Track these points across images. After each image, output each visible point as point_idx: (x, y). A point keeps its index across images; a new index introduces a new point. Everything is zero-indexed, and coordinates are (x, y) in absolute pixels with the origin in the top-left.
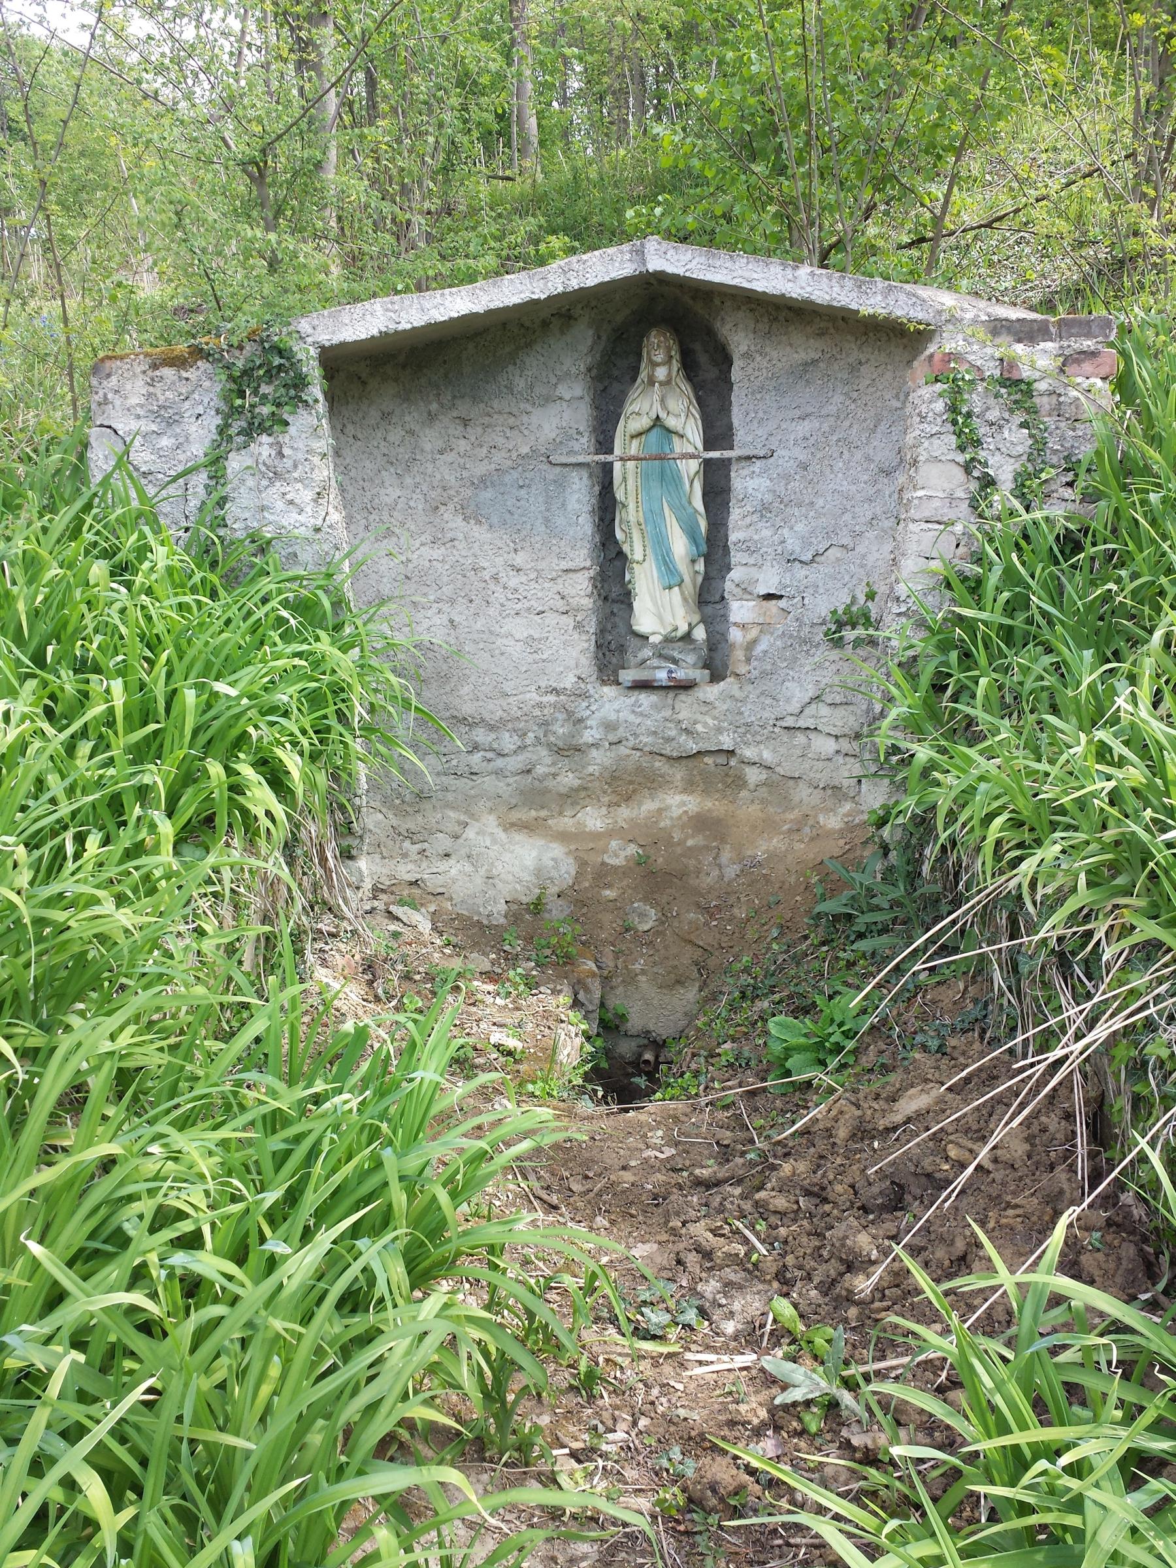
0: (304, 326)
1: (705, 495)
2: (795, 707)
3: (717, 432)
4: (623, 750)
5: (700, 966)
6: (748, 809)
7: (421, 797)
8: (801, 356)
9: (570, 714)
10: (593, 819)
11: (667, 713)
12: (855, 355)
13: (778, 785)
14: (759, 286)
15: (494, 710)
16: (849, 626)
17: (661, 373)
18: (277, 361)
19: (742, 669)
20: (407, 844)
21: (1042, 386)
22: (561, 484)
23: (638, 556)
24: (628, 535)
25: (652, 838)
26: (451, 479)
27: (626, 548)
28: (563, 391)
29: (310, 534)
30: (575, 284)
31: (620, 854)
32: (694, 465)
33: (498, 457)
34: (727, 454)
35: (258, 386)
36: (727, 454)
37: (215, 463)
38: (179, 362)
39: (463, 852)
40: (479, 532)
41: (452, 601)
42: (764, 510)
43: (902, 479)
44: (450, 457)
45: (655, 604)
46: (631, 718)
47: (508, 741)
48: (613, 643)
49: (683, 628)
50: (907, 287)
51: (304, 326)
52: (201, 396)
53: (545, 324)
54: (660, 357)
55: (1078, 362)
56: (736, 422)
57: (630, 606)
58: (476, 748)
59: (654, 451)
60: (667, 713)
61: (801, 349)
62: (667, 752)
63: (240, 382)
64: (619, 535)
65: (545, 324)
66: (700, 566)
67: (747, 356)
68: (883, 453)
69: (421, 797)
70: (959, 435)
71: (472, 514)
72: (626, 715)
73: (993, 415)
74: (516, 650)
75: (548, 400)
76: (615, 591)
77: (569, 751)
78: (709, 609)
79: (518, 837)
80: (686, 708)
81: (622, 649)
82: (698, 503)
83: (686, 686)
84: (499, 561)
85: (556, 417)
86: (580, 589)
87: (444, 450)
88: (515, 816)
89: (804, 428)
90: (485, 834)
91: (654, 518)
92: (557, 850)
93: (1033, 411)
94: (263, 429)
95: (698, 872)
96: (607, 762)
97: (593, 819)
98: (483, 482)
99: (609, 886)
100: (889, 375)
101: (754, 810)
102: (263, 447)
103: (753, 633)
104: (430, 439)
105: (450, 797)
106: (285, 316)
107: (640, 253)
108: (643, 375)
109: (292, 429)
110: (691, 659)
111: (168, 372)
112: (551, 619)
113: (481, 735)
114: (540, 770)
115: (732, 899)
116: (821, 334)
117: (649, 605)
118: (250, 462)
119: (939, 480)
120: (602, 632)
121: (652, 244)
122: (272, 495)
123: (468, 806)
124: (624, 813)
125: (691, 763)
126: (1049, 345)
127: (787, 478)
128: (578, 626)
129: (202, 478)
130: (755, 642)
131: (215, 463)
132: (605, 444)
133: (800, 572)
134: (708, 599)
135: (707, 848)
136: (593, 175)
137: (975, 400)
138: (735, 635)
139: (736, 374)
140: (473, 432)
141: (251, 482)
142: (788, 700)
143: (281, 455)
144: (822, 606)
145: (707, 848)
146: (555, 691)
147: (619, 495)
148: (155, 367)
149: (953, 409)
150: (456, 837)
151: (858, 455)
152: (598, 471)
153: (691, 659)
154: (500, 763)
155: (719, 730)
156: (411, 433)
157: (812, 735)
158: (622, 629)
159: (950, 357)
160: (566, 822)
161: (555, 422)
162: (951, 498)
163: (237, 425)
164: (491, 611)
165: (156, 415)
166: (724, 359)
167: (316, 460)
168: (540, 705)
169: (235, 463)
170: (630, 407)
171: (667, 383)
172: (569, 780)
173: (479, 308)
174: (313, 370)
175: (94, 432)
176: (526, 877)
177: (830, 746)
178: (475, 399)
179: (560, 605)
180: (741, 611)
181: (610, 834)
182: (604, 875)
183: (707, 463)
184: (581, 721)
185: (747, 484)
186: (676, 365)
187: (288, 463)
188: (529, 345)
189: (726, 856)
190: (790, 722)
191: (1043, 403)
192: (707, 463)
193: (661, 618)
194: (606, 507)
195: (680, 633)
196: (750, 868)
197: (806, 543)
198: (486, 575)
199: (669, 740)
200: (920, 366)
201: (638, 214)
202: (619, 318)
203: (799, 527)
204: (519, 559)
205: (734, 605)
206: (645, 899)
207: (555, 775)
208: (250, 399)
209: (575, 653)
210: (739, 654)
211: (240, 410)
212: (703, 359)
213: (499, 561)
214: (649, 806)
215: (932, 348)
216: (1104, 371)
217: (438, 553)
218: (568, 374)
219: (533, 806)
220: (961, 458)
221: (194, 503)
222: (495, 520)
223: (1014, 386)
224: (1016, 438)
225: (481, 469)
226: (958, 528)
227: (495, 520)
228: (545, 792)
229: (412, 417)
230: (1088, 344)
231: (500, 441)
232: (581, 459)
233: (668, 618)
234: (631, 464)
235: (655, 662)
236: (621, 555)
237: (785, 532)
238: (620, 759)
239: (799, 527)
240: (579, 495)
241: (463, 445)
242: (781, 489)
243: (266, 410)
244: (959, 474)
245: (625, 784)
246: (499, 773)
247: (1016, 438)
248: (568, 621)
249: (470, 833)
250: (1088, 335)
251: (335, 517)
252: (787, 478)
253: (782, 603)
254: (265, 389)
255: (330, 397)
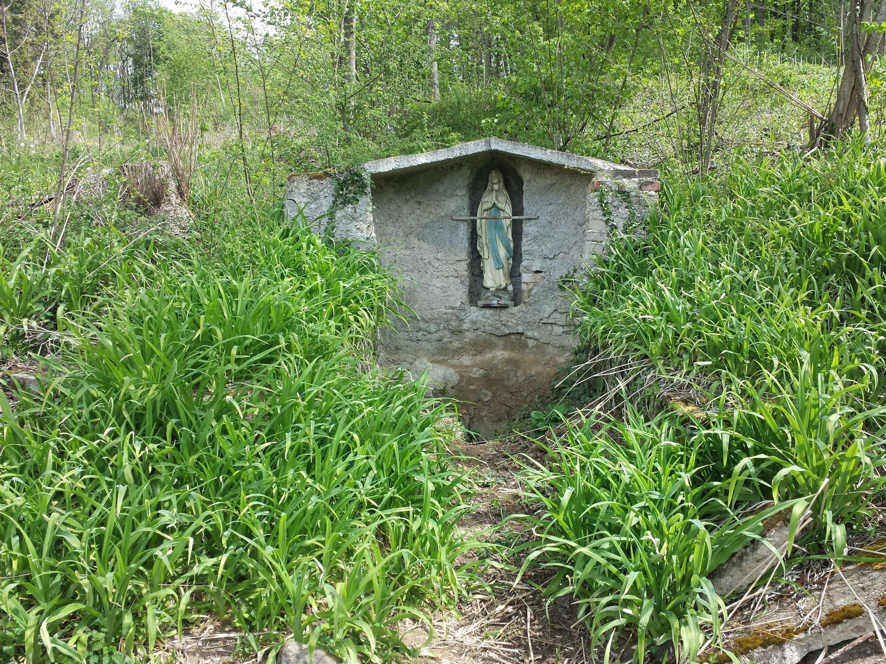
0: (366, 166)
1: (513, 234)
2: (547, 315)
3: (517, 209)
4: (479, 333)
5: (508, 414)
6: (528, 356)
7: (397, 348)
8: (549, 182)
9: (458, 317)
10: (466, 360)
11: (497, 317)
12: (569, 182)
13: (541, 346)
14: (533, 156)
15: (428, 315)
16: (565, 283)
17: (496, 187)
18: (356, 178)
19: (527, 300)
20: (392, 365)
21: (633, 194)
22: (456, 227)
23: (486, 256)
24: (482, 248)
25: (489, 368)
26: (414, 224)
27: (481, 253)
28: (458, 192)
29: (365, 240)
30: (464, 153)
31: (477, 373)
32: (508, 222)
33: (432, 216)
34: (521, 217)
35: (348, 187)
36: (521, 217)
37: (331, 214)
38: (319, 178)
39: (414, 370)
40: (424, 245)
41: (412, 271)
42: (535, 239)
43: (584, 227)
44: (413, 216)
45: (492, 274)
46: (483, 319)
47: (433, 328)
48: (475, 289)
49: (504, 285)
50: (585, 158)
51: (366, 166)
52: (326, 192)
53: (452, 168)
54: (495, 182)
55: (646, 185)
56: (524, 206)
57: (483, 277)
58: (420, 330)
59: (493, 216)
60: (497, 317)
61: (550, 180)
62: (497, 333)
63: (342, 185)
64: (478, 248)
65: (452, 168)
66: (511, 261)
67: (529, 181)
68: (579, 219)
69: (397, 348)
70: (603, 210)
71: (421, 238)
72: (480, 318)
73: (615, 204)
74: (437, 291)
75: (452, 196)
76: (477, 271)
77: (457, 332)
78: (514, 279)
79: (436, 365)
80: (504, 315)
81: (479, 294)
82: (510, 237)
83: (505, 307)
84: (431, 256)
85: (456, 202)
86: (463, 268)
87: (412, 214)
88: (434, 358)
89: (550, 208)
90: (423, 363)
91: (492, 241)
92: (452, 371)
93: (630, 202)
94: (349, 202)
95: (508, 379)
96: (472, 337)
97: (466, 360)
98: (426, 226)
99: (472, 384)
100: (581, 189)
101: (531, 357)
102: (349, 209)
103: (531, 286)
104: (406, 209)
105: (409, 349)
106: (357, 162)
107: (489, 143)
108: (489, 187)
109: (360, 203)
110: (506, 297)
111: (315, 181)
112: (451, 279)
113: (422, 325)
114: (445, 340)
115: (521, 389)
116: (556, 174)
117: (490, 276)
118: (344, 214)
119: (596, 226)
120: (471, 286)
121: (493, 140)
122: (352, 226)
123: (416, 355)
124: (479, 358)
125: (506, 338)
126: (636, 179)
127: (544, 227)
128: (462, 282)
129: (326, 219)
130: (531, 289)
131: (331, 214)
132: (474, 212)
133: (549, 262)
134: (514, 275)
135: (512, 370)
136: (467, 101)
137: (609, 198)
138: (524, 287)
139: (524, 188)
140: (423, 207)
141: (344, 221)
142: (544, 312)
143: (356, 212)
144: (556, 275)
145: (512, 370)
146: (452, 308)
147: (479, 233)
148: (311, 179)
149: (601, 201)
150: (412, 364)
151: (570, 219)
152: (470, 223)
153: (506, 297)
154: (429, 336)
155: (517, 324)
156: (399, 207)
157: (554, 326)
158: (479, 286)
159: (600, 183)
160: (455, 361)
161: (455, 204)
162: (601, 233)
163: (340, 200)
164: (427, 276)
165: (310, 196)
166: (520, 182)
167: (368, 214)
168: (446, 313)
169: (338, 214)
170: (484, 199)
171: (498, 191)
172: (457, 344)
173: (429, 161)
174: (368, 181)
175: (286, 202)
176: (439, 380)
177: (561, 330)
178: (424, 195)
179: (455, 274)
180: (526, 277)
181: (473, 366)
182: (470, 381)
183: (514, 221)
184: (462, 320)
185: (529, 229)
186: (502, 184)
187: (358, 215)
188: (445, 175)
189: (519, 373)
190: (545, 321)
191: (634, 199)
192: (514, 221)
193: (495, 281)
194: (474, 237)
195: (502, 287)
196: (529, 379)
197: (551, 251)
198: (426, 262)
199: (497, 328)
200: (590, 186)
201: (487, 122)
202: (480, 166)
203: (548, 245)
204: (439, 256)
205: (524, 275)
206: (487, 389)
207: (451, 342)
208: (345, 191)
209: (460, 293)
210: (526, 294)
211: (341, 195)
212: (513, 182)
213: (431, 256)
214: (489, 355)
215: (594, 179)
216: (656, 189)
217: (407, 252)
218: (460, 186)
219: (442, 354)
220: (605, 219)
221: (323, 228)
222: (430, 240)
223: (622, 192)
224: (624, 212)
225: (425, 221)
226: (603, 244)
227: (430, 240)
228: (447, 349)
229: (400, 201)
230: (650, 179)
231: (433, 210)
232: (464, 218)
233: (498, 281)
234: (484, 221)
235: (492, 298)
236: (479, 257)
237: (543, 247)
238: (478, 336)
239: (548, 245)
240: (463, 232)
241: (418, 212)
242: (541, 231)
243: (351, 195)
244: (604, 224)
245: (480, 346)
246: (428, 341)
247: (624, 212)
248: (458, 280)
249: (417, 363)
250: (650, 176)
251: (374, 235)
252: (544, 227)
253: (542, 274)
254: (350, 188)
255: (374, 192)
